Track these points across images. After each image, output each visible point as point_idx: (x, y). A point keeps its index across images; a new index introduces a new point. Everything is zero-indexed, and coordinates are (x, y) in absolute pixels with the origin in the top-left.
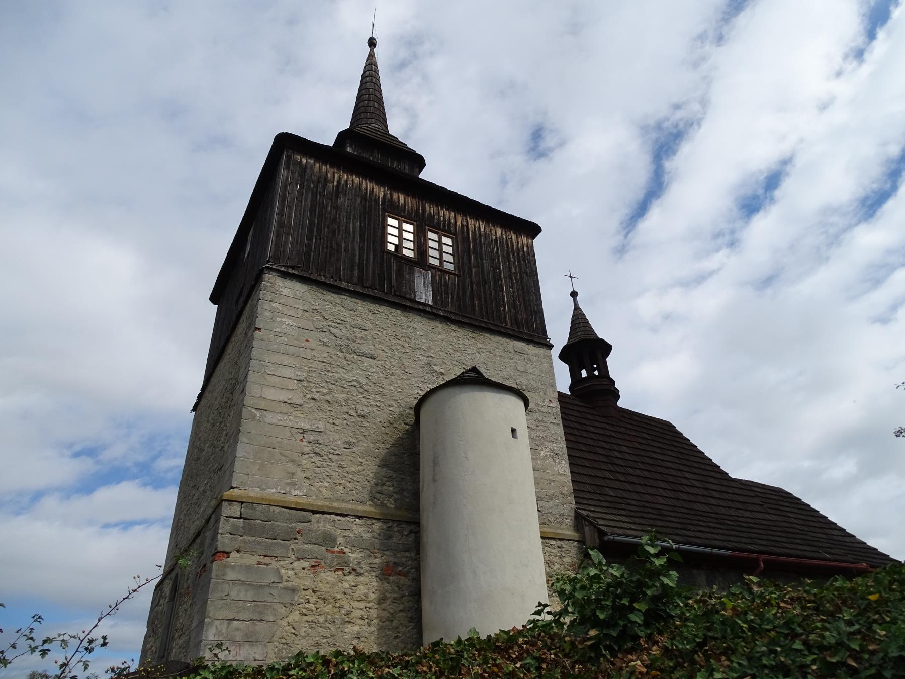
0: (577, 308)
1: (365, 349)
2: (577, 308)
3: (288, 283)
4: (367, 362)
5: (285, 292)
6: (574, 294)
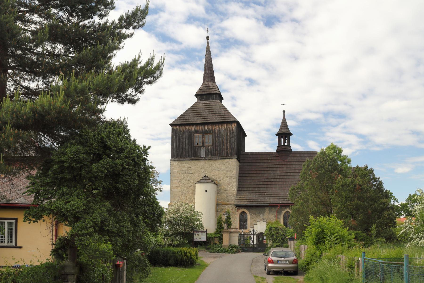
0: (284, 118)
1: (191, 172)
2: (284, 118)
3: (175, 162)
4: (191, 175)
5: (174, 164)
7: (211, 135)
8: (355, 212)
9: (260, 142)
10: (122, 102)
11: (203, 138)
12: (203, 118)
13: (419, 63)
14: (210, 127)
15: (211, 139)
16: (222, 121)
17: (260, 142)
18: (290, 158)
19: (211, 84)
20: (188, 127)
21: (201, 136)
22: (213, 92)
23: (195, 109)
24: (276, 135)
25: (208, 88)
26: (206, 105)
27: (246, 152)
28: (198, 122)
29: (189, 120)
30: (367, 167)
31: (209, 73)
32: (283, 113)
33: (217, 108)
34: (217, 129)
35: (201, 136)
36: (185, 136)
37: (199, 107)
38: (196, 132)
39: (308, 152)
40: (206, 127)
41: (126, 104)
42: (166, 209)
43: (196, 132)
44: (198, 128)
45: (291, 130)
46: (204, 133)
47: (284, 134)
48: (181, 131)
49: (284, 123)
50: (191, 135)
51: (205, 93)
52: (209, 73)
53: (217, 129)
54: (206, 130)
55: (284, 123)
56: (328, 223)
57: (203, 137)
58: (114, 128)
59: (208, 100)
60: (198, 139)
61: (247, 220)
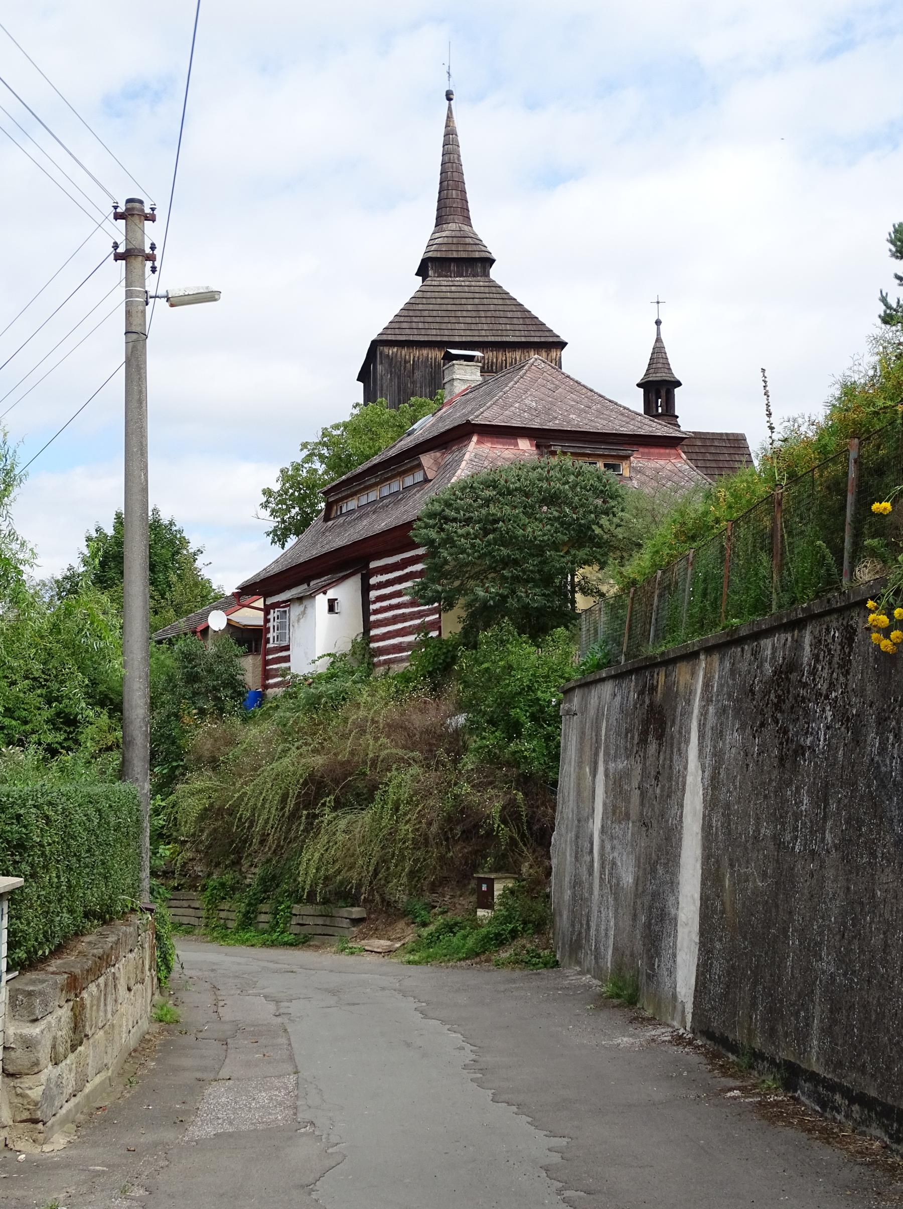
0: (658, 340)
2: (658, 340)
6: (658, 323)
10: (472, 489)
12: (467, 327)
16: (523, 339)
19: (466, 228)
20: (425, 352)
22: (477, 255)
23: (433, 301)
24: (639, 385)
25: (462, 240)
26: (459, 289)
28: (457, 339)
29: (429, 332)
31: (452, 201)
33: (496, 302)
36: (418, 375)
37: (442, 295)
39: (721, 434)
41: (343, 399)
45: (678, 373)
48: (406, 362)
49: (658, 356)
51: (455, 255)
52: (452, 201)
55: (658, 356)
58: (25, 899)
59: (462, 276)
61: (692, 713)
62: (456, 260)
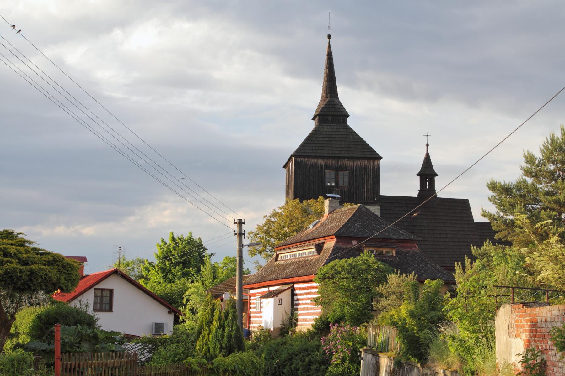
0: (428, 155)
2: (428, 155)
7: (346, 173)
8: (475, 326)
9: (398, 182)
11: (336, 176)
13: (473, 373)
14: (347, 163)
15: (347, 177)
17: (398, 182)
18: (475, 248)
20: (316, 160)
21: (333, 173)
24: (417, 175)
27: (381, 194)
30: (530, 159)
32: (426, 147)
34: (355, 165)
35: (333, 173)
38: (327, 167)
40: (341, 162)
42: (159, 263)
43: (327, 167)
44: (330, 162)
46: (337, 169)
47: (427, 174)
49: (427, 161)
50: (320, 170)
53: (355, 165)
54: (341, 166)
55: (427, 161)
56: (335, 369)
57: (337, 175)
60: (329, 175)
62: (331, 114)
